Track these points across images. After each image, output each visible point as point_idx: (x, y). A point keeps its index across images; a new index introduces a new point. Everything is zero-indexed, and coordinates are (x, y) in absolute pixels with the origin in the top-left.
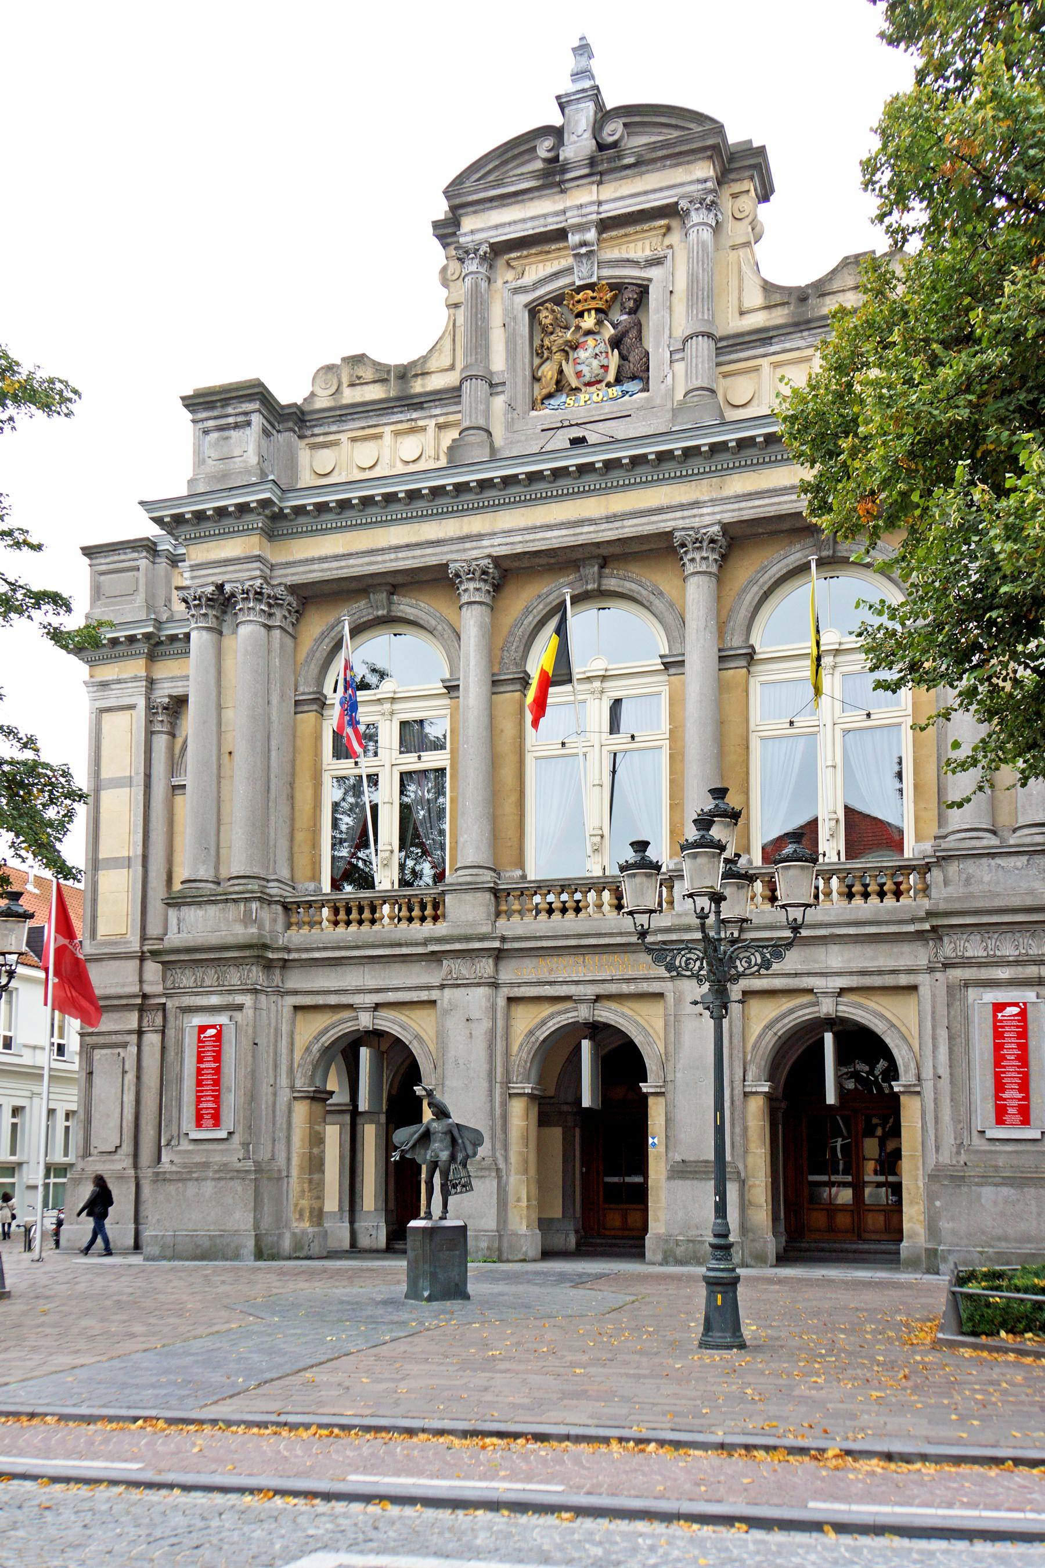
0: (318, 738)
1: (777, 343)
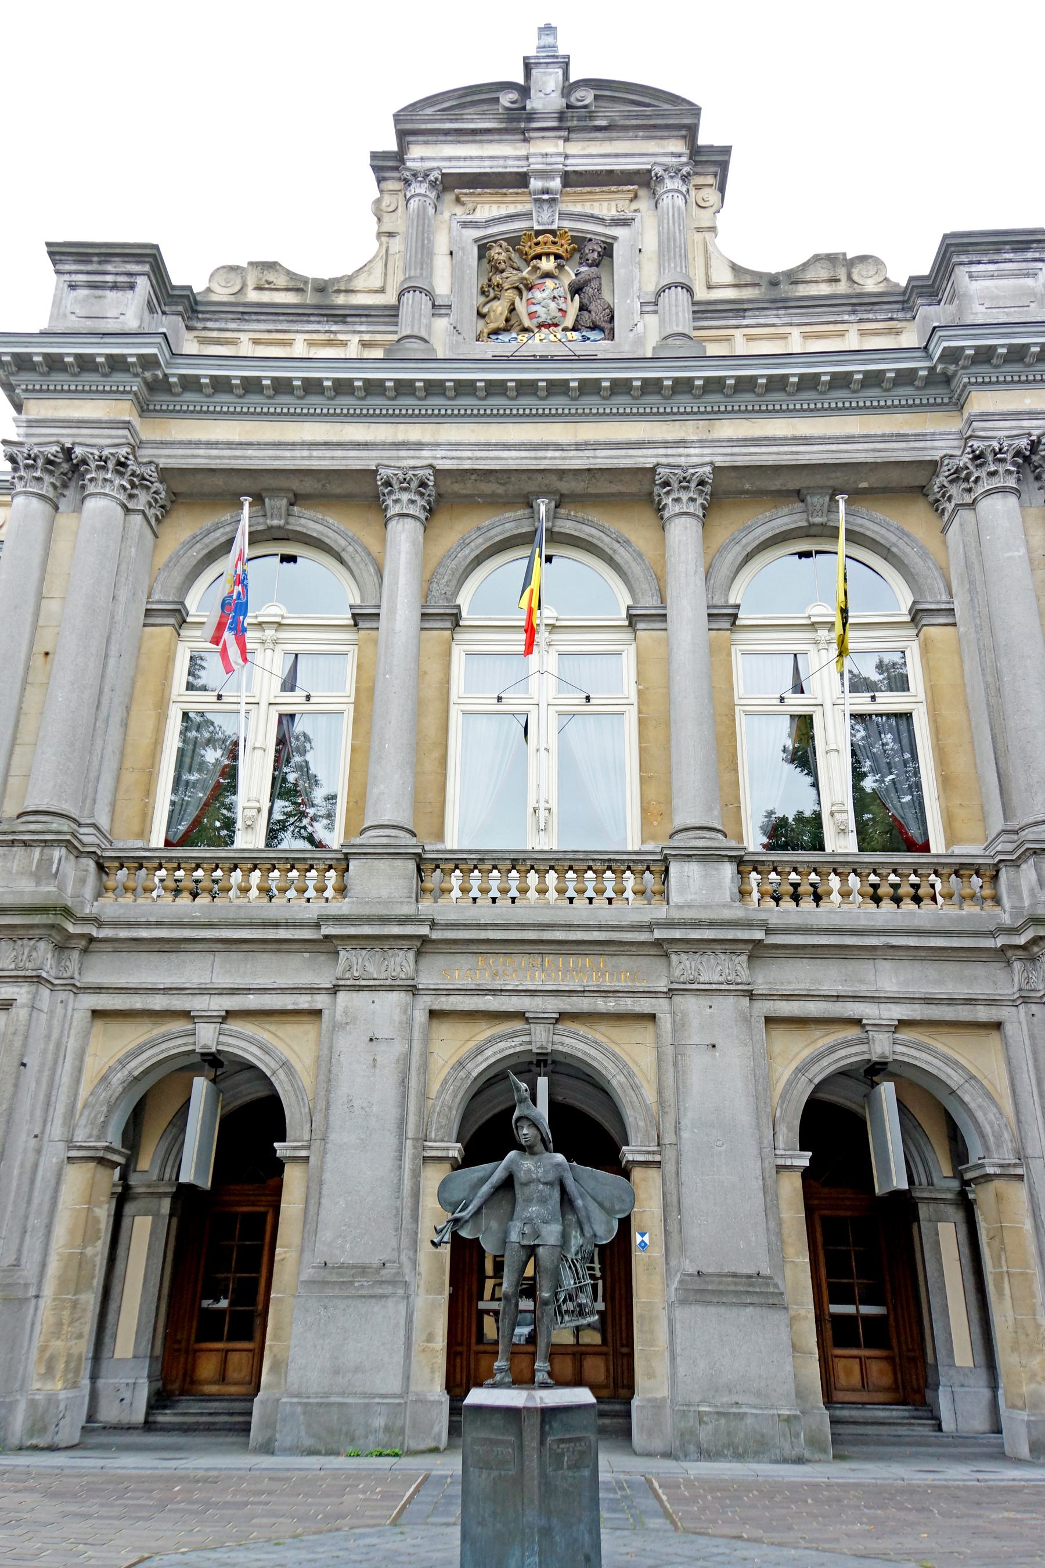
0: (170, 659)
1: (751, 317)
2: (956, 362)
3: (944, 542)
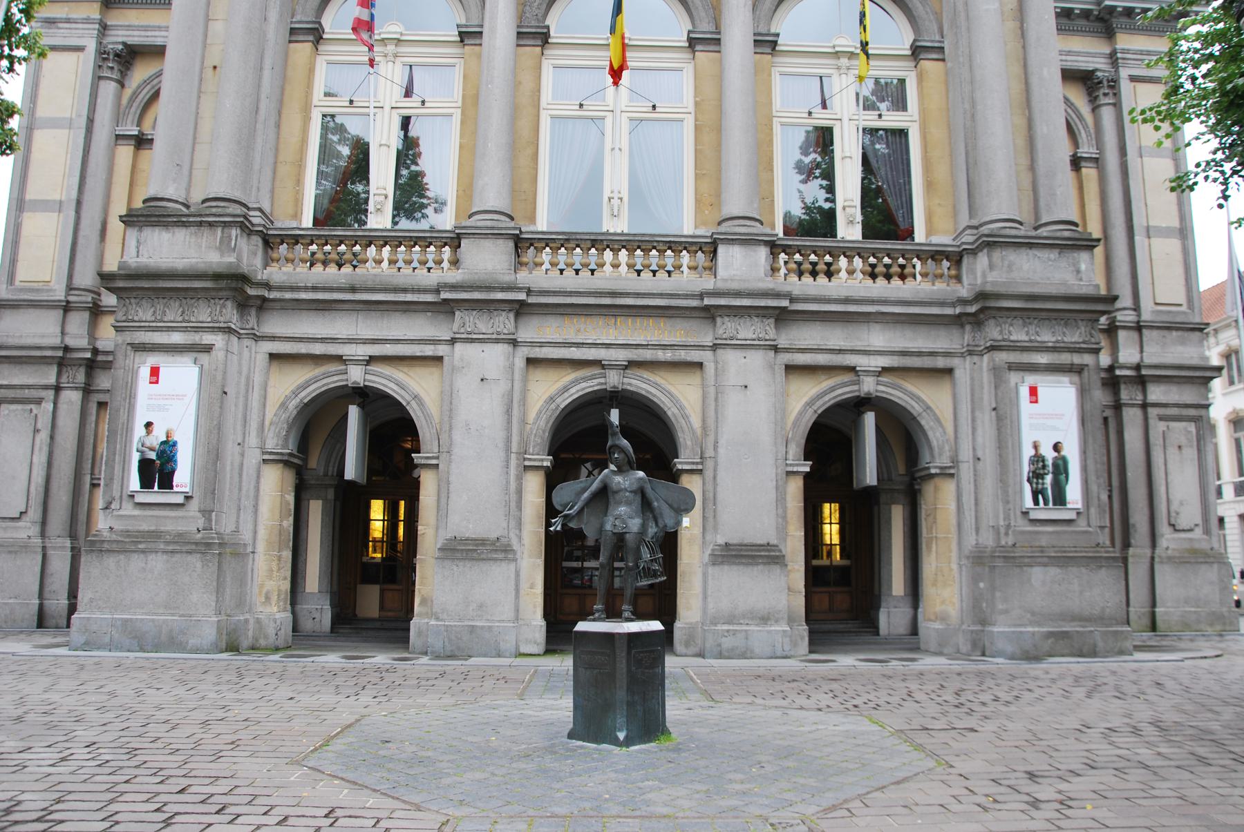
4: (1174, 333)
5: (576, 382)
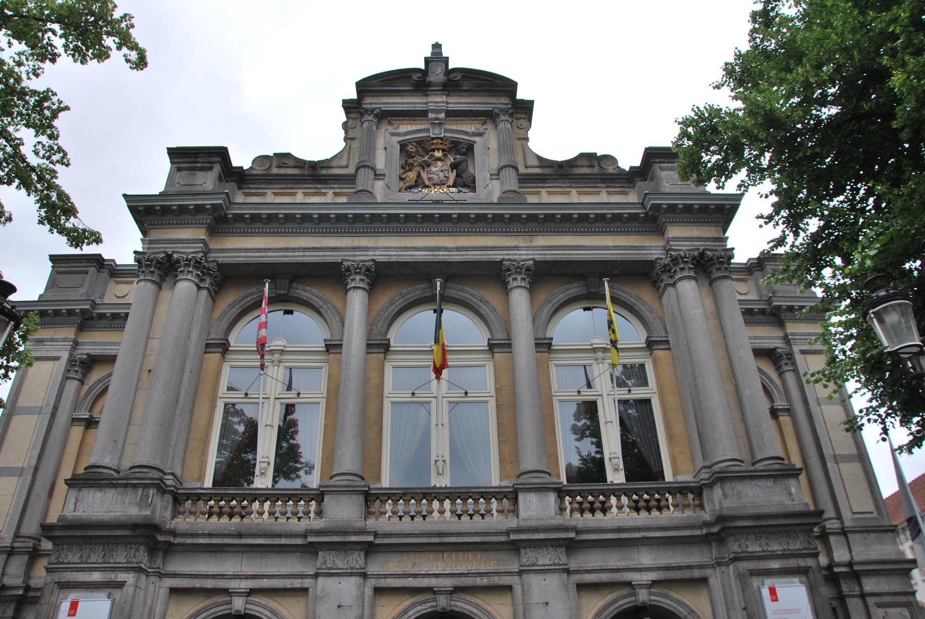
2: (658, 211)
3: (661, 303)
4: (872, 535)
5: (413, 606)
